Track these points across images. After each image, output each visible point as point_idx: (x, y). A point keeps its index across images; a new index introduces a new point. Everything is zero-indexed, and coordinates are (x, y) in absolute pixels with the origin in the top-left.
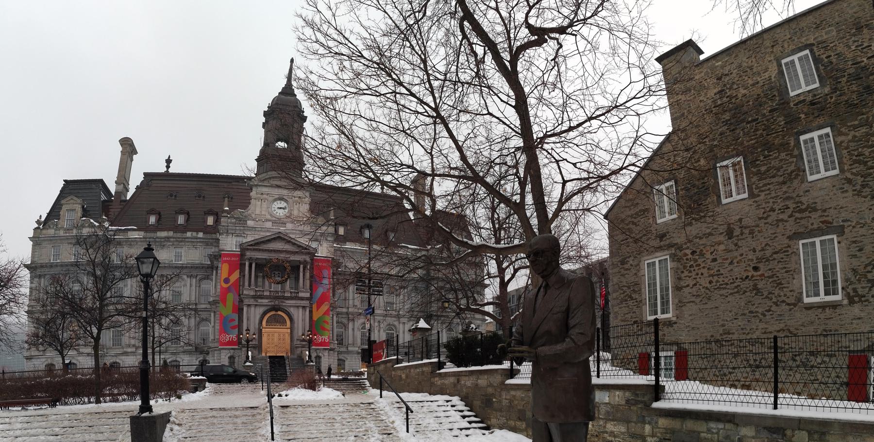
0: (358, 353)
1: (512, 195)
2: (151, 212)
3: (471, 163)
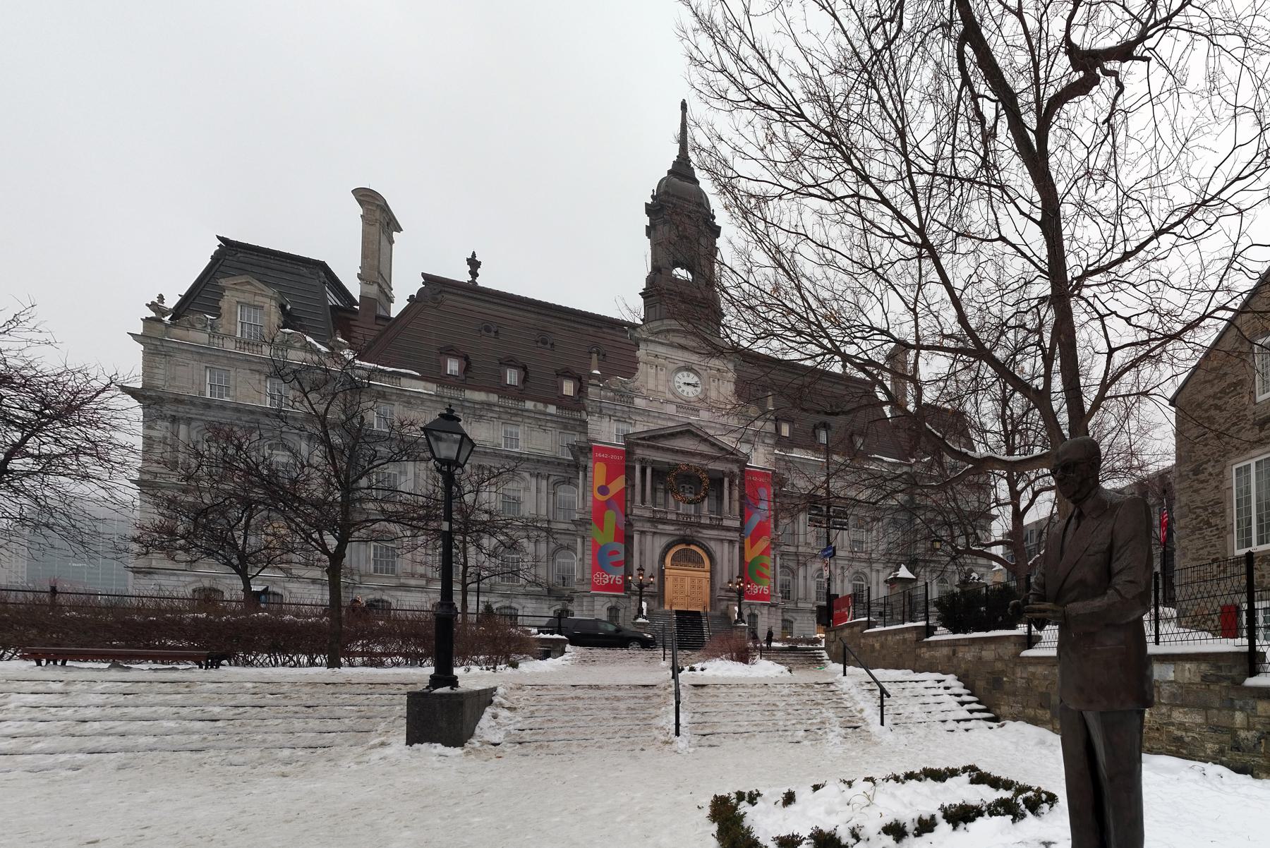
0: (812, 612)
1: (1033, 378)
2: (450, 352)
3: (973, 326)
